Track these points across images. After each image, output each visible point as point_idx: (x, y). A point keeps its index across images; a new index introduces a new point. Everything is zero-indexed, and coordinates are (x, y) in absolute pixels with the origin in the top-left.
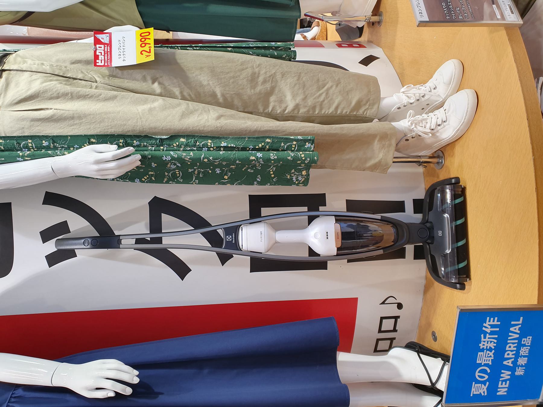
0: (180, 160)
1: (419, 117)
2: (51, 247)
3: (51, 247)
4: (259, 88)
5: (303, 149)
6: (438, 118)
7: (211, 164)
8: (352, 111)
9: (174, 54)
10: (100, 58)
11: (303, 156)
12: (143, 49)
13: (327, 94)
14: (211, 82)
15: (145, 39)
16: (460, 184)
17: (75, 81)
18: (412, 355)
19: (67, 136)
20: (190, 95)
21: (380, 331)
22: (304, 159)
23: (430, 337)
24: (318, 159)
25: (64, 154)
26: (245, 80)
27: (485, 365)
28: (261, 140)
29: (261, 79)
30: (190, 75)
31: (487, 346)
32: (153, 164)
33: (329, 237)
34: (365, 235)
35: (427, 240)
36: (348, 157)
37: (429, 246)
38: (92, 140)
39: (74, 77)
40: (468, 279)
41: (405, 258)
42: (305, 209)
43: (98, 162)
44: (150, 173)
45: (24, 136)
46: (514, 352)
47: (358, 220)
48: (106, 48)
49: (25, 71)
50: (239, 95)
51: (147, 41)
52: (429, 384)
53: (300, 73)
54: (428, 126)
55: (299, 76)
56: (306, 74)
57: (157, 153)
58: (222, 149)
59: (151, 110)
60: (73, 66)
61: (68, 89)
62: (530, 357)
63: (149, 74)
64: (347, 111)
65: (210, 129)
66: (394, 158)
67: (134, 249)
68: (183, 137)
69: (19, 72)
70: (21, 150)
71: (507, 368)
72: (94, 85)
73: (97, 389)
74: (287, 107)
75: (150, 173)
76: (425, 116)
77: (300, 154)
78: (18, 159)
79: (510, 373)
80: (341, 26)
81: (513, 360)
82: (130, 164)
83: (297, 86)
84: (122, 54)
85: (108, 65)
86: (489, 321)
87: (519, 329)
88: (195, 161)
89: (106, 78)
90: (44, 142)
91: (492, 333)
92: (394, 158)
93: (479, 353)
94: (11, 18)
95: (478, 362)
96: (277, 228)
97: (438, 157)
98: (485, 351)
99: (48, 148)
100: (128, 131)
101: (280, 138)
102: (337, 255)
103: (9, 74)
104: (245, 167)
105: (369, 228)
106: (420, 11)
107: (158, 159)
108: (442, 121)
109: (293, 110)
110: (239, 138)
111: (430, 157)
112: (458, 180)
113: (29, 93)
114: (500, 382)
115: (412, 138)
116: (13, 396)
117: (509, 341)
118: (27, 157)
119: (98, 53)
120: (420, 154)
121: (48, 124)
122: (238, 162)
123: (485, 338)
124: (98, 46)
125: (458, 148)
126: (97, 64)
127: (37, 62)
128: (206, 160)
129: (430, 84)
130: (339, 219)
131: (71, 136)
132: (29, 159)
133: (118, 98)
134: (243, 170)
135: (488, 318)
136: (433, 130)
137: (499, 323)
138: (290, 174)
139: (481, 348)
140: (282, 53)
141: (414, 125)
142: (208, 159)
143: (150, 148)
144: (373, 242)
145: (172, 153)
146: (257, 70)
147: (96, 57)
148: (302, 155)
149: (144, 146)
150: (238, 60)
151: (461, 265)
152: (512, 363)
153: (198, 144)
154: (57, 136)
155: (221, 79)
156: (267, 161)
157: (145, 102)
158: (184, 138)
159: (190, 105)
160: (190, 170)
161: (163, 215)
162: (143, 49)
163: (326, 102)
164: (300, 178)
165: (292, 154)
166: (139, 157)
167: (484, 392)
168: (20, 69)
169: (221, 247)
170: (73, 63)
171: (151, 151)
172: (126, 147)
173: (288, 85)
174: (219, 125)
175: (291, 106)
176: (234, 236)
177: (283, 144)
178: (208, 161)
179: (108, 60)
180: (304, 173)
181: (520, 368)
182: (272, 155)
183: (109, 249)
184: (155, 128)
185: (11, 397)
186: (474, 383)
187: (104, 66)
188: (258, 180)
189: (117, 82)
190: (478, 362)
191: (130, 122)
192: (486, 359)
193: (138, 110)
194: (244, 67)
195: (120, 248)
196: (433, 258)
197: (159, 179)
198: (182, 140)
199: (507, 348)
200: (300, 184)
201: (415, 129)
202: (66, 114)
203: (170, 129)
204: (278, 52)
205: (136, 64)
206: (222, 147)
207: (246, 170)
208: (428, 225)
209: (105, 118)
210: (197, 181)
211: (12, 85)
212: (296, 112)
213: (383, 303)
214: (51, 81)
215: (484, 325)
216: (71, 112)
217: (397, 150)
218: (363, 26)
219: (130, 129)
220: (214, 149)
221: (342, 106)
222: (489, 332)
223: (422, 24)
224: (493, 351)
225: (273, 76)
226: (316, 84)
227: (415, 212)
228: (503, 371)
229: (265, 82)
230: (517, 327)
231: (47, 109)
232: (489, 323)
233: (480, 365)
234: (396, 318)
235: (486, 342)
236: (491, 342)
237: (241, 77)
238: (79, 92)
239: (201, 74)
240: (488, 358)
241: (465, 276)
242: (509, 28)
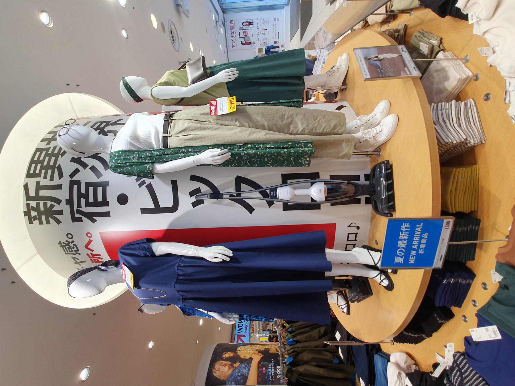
0: (248, 154)
1: (367, 131)
2: (194, 199)
3: (194, 199)
4: (285, 122)
5: (307, 147)
6: (377, 130)
7: (262, 156)
8: (332, 130)
9: (245, 108)
10: (212, 112)
11: (307, 150)
12: (231, 106)
13: (319, 122)
14: (262, 120)
15: (232, 101)
17: (202, 122)
18: (366, 251)
19: (199, 146)
20: (252, 126)
21: (348, 240)
22: (307, 151)
23: (374, 243)
24: (314, 151)
25: (198, 154)
26: (278, 118)
27: (403, 248)
28: (286, 143)
29: (286, 117)
30: (253, 117)
31: (403, 238)
32: (236, 157)
33: (321, 191)
34: (339, 191)
35: (372, 193)
36: (330, 152)
37: (373, 197)
38: (210, 147)
39: (202, 120)
40: (394, 211)
41: (360, 203)
42: (310, 179)
43: (212, 156)
44: (235, 162)
45: (182, 147)
46: (418, 241)
47: (336, 184)
48: (215, 107)
49: (181, 119)
50: (275, 125)
51: (233, 102)
52: (373, 264)
53: (305, 113)
54: (371, 135)
55: (305, 114)
56: (308, 113)
57: (238, 152)
58: (268, 148)
59: (235, 133)
60: (201, 116)
61: (199, 125)
62: (427, 244)
63: (234, 117)
64: (329, 130)
65: (262, 140)
66: (354, 153)
67: (229, 200)
68: (250, 144)
69: (179, 120)
70: (180, 154)
71: (414, 250)
72: (210, 123)
73: (215, 258)
74: (299, 129)
75: (235, 162)
76: (370, 130)
77: (306, 149)
78: (179, 157)
79: (416, 252)
80: (326, 94)
81: (417, 245)
82: (226, 157)
83: (304, 119)
84: (222, 109)
85: (216, 115)
86: (404, 225)
87: (421, 229)
88: (255, 154)
89: (215, 120)
90: (189, 149)
91: (406, 231)
92: (354, 153)
93: (399, 241)
94: (175, 102)
95: (398, 246)
96: (295, 188)
97: (378, 151)
98: (402, 240)
99: (191, 152)
100: (225, 143)
101: (296, 142)
102: (326, 200)
103: (175, 121)
104: (279, 157)
105: (342, 187)
106: (366, 74)
107: (238, 155)
108: (379, 131)
109: (302, 131)
110: (276, 143)
111: (373, 152)
112: (388, 161)
113: (183, 128)
114: (410, 257)
115: (363, 141)
116: (181, 260)
117: (415, 236)
118: (183, 156)
119: (211, 110)
120: (368, 150)
121: (191, 141)
122: (275, 154)
123: (402, 233)
124: (211, 106)
125: (388, 146)
126: (211, 114)
127: (186, 115)
128: (260, 154)
129: (373, 114)
130: (326, 183)
131: (200, 146)
132: (184, 157)
133: (220, 128)
134: (278, 158)
135: (404, 223)
136: (374, 136)
137: (410, 226)
138: (301, 160)
139: (400, 239)
140: (296, 104)
141: (364, 134)
142: (261, 153)
143: (235, 150)
144: (344, 194)
145: (245, 151)
146: (284, 113)
147: (211, 111)
148: (306, 149)
149: (232, 149)
150: (275, 109)
151: (390, 204)
152: (417, 247)
153: (256, 147)
154: (195, 146)
155: (267, 118)
156: (290, 153)
157: (233, 129)
158: (250, 144)
159: (253, 130)
160: (253, 160)
162: (231, 106)
163: (318, 126)
164: (306, 162)
165: (302, 149)
166: (230, 153)
167: (402, 262)
168: (179, 118)
169: (268, 198)
170: (201, 115)
171: (235, 151)
172: (224, 149)
173: (299, 119)
174: (266, 138)
175: (301, 129)
176: (274, 192)
177: (297, 145)
178: (261, 154)
180: (308, 159)
181: (421, 250)
182: (292, 150)
183: (219, 199)
184: (237, 141)
185: (180, 261)
186: (396, 257)
187: (214, 115)
188: (286, 163)
189: (220, 122)
190: (398, 246)
191: (226, 139)
192: (403, 244)
193: (229, 133)
194: (278, 112)
195: (223, 199)
196: (375, 202)
197: (239, 165)
198: (249, 145)
199: (414, 239)
200: (307, 165)
201: (364, 136)
202: (199, 136)
203: (244, 141)
204: (294, 104)
205: (228, 113)
206: (267, 147)
207: (279, 159)
208: (372, 185)
209: (215, 137)
210: (256, 165)
211: (176, 126)
212: (303, 132)
213: (349, 226)
214: (192, 122)
215: (402, 227)
216: (201, 135)
217: (355, 148)
218: (338, 91)
219: (226, 141)
220: (264, 149)
221: (326, 128)
222: (404, 230)
223: (367, 80)
224: (407, 241)
225: (292, 115)
227: (366, 180)
228: (412, 251)
229: (288, 118)
230: (420, 228)
231: (191, 134)
232: (404, 226)
233: (399, 248)
234: (356, 234)
235: (403, 236)
236: (405, 236)
237: (277, 116)
238: (204, 126)
239: (257, 116)
240: (404, 244)
241: (392, 209)
242: (414, 78)
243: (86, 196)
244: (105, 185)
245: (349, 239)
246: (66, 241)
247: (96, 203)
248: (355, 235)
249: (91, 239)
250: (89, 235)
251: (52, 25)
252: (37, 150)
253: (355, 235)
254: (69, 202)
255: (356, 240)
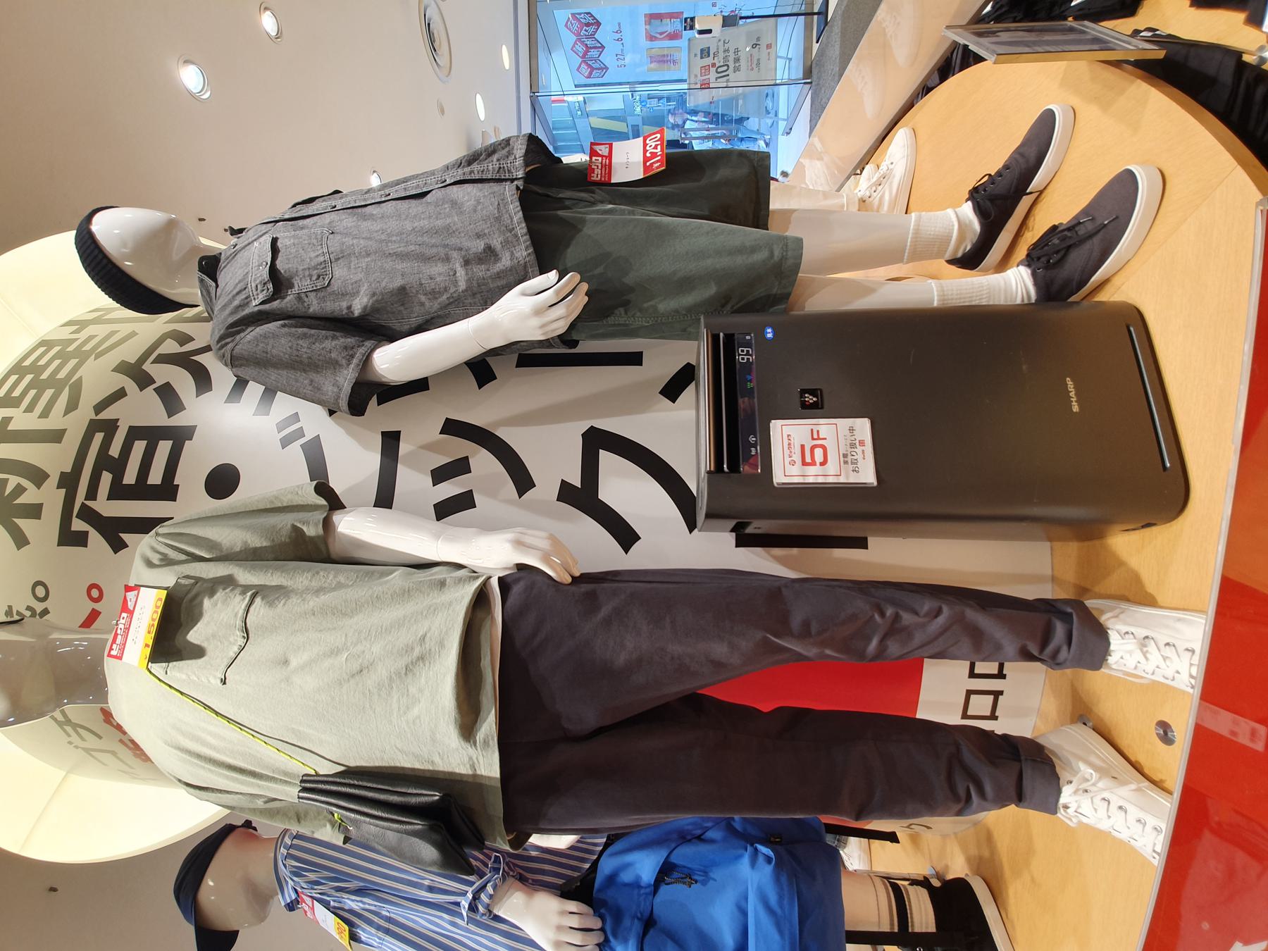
10: (596, 172)
16: (315, 482)
124: (594, 158)
161: (103, 434)
179: (605, 174)
226: (1020, 293)
243: (118, 468)
244: (180, 436)
245: (969, 713)
246: (28, 606)
247: (142, 491)
248: (992, 697)
249: (97, 606)
250: (95, 593)
251: (207, 95)
252: (43, 343)
253: (991, 697)
254: (68, 482)
255: (996, 718)
